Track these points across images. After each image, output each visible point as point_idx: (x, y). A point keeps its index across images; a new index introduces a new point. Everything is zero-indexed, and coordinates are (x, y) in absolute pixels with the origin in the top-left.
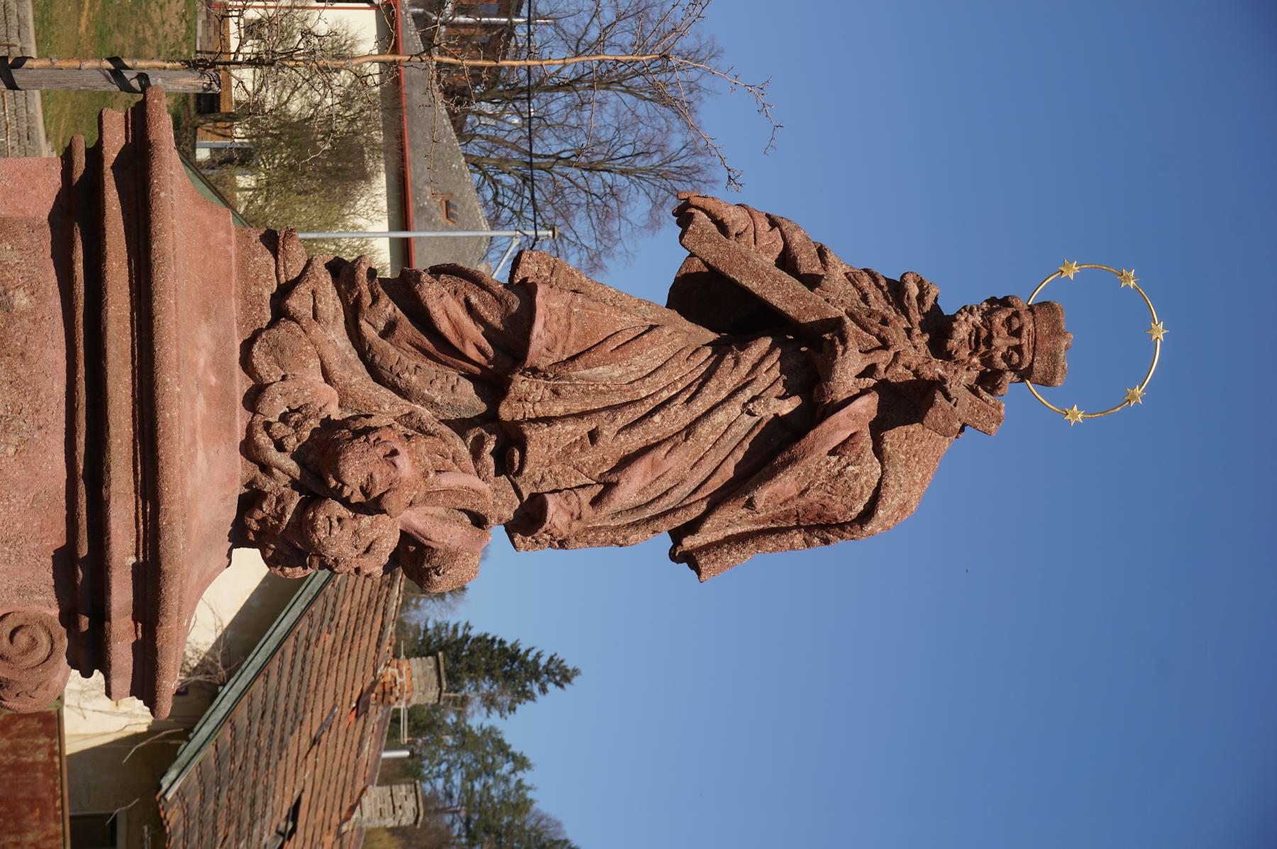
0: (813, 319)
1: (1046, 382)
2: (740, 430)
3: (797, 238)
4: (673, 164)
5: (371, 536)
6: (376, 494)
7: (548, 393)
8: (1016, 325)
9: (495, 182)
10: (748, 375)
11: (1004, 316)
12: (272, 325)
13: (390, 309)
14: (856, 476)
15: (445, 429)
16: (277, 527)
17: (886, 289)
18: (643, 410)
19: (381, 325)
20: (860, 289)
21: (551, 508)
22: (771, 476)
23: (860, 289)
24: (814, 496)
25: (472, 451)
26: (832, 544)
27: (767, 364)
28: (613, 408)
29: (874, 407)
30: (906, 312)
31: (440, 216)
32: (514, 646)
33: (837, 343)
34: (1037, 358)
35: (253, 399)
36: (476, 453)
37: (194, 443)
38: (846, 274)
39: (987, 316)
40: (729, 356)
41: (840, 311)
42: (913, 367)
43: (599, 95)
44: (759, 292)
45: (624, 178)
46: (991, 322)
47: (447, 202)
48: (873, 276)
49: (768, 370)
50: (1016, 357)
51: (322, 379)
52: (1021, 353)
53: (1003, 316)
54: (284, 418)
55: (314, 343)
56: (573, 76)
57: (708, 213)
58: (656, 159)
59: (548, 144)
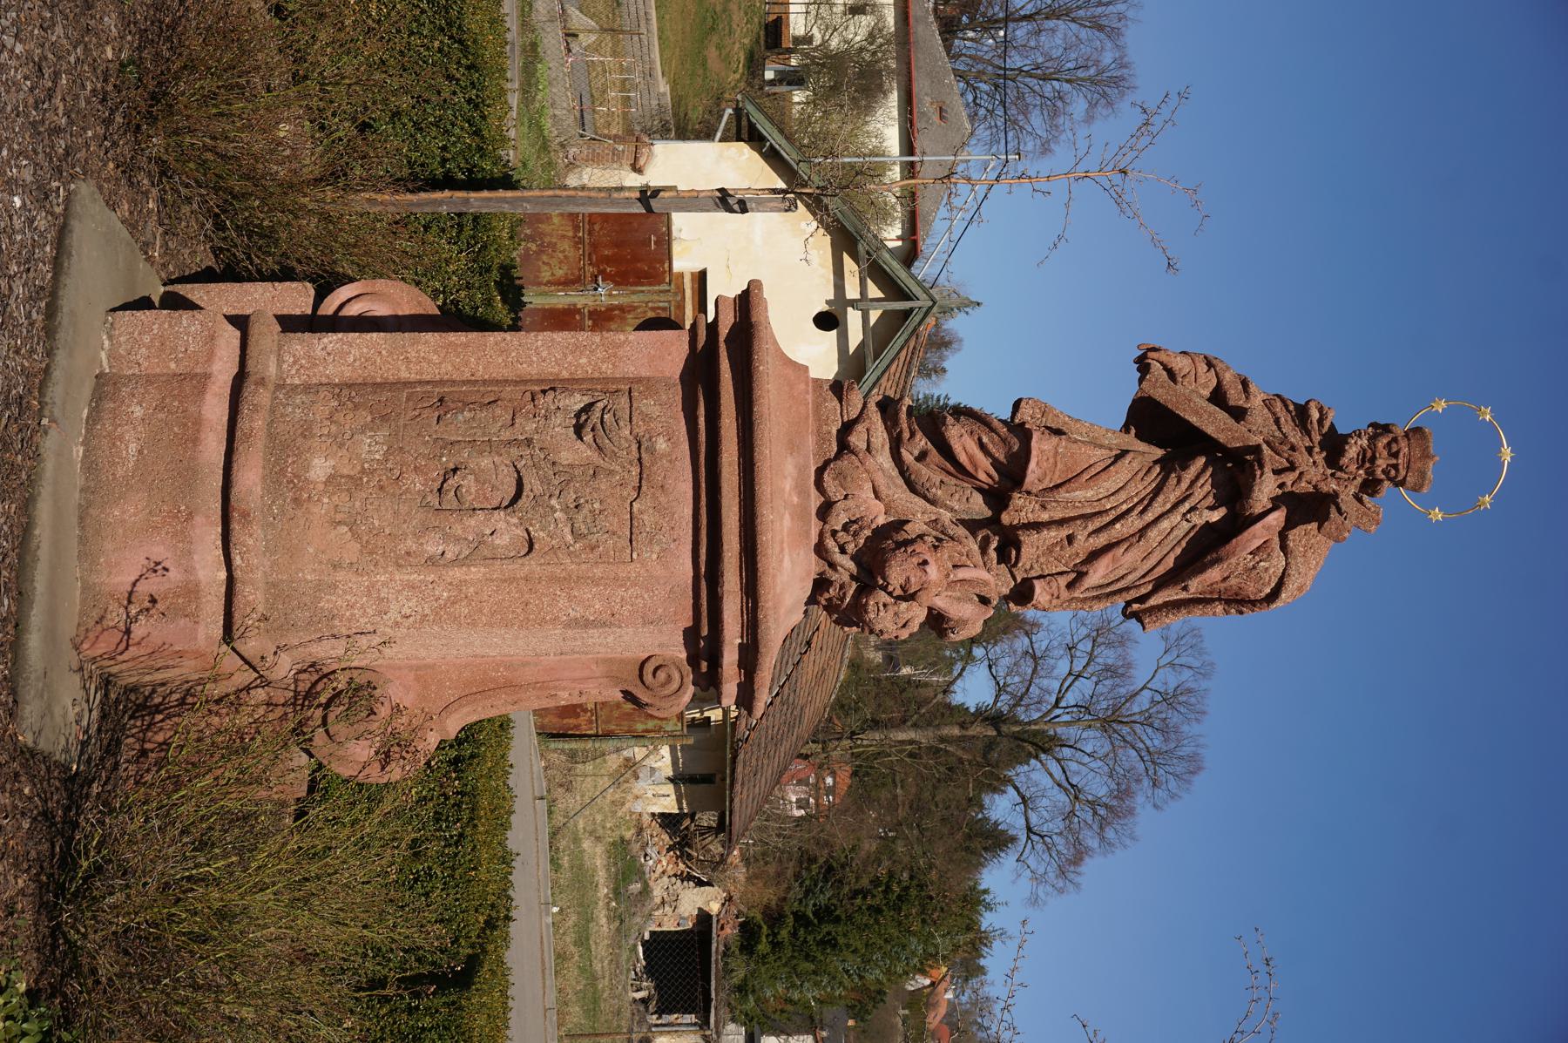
0: (1238, 445)
1: (1416, 489)
2: (1179, 533)
3: (1228, 377)
4: (1105, 75)
5: (907, 616)
6: (912, 591)
7: (1037, 506)
9: (975, 89)
10: (1187, 490)
11: (1385, 441)
12: (838, 456)
13: (923, 443)
14: (1267, 570)
15: (961, 531)
16: (840, 606)
17: (1293, 414)
18: (1107, 519)
19: (916, 453)
20: (1274, 414)
21: (1038, 590)
22: (1202, 570)
23: (1274, 414)
24: (1233, 581)
25: (980, 547)
26: (1245, 615)
28: (1086, 517)
31: (935, 118)
33: (1256, 467)
34: (1410, 474)
35: (825, 511)
36: (984, 549)
37: (782, 550)
38: (1264, 401)
39: (1373, 439)
40: (1173, 475)
41: (1258, 439)
42: (1314, 483)
43: (1051, 24)
44: (1197, 424)
45: (1068, 85)
46: (1375, 445)
47: (941, 108)
48: (1283, 401)
49: (1203, 485)
50: (1393, 472)
51: (873, 496)
52: (1397, 470)
54: (845, 528)
55: (867, 471)
56: (1034, 10)
57: (1161, 363)
58: (1092, 71)
59: (1015, 61)
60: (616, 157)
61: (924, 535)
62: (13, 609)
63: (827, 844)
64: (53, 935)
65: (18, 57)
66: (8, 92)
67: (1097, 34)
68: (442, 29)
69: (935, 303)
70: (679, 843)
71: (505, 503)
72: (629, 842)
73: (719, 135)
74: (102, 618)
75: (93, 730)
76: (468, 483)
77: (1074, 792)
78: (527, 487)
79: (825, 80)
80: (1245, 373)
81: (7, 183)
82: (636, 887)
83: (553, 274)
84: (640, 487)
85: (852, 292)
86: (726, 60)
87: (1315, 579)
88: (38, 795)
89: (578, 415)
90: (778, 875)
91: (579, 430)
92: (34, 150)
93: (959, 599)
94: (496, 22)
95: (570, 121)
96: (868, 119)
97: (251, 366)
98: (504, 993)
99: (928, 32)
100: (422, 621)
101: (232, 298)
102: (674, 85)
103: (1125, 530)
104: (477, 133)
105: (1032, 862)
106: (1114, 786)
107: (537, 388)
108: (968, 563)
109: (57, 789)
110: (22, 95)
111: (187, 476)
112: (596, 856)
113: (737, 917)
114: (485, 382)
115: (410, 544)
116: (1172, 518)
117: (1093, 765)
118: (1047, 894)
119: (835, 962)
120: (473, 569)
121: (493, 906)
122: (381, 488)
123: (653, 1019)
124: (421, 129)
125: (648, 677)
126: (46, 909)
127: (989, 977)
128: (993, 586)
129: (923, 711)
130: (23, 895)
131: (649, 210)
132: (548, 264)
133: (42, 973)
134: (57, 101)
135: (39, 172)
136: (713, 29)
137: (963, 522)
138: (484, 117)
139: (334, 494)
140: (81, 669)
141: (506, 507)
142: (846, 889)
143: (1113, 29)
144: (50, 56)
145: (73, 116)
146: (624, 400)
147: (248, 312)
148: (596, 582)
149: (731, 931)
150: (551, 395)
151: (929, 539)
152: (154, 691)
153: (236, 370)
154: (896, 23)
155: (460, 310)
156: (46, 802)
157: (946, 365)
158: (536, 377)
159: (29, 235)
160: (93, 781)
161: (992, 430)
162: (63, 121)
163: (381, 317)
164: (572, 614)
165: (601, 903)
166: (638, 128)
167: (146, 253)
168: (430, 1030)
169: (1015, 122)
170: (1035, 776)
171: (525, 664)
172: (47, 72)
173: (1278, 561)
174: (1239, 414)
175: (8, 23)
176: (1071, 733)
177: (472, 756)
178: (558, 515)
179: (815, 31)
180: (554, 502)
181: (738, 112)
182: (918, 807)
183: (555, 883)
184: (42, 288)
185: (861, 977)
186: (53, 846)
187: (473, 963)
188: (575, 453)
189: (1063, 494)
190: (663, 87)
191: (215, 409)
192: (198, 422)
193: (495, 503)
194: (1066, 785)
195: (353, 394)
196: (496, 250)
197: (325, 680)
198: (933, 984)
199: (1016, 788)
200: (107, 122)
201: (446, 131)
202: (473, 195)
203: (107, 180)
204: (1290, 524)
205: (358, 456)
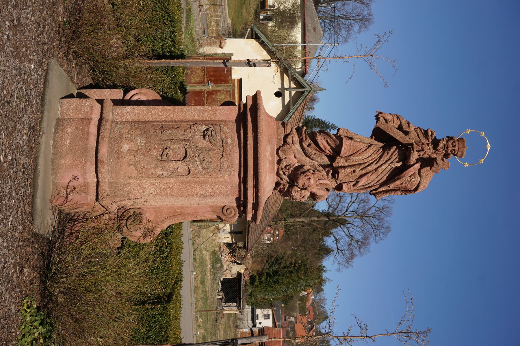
1: (460, 157)
2: (387, 170)
3: (403, 122)
5: (304, 195)
6: (305, 187)
7: (344, 161)
8: (454, 144)
9: (324, 22)
12: (284, 145)
14: (414, 181)
15: (321, 168)
18: (365, 165)
19: (307, 144)
20: (417, 133)
21: (344, 187)
22: (394, 181)
23: (417, 133)
24: (404, 185)
25: (327, 173)
27: (395, 154)
29: (419, 166)
30: (428, 139)
31: (312, 31)
32: (324, 121)
35: (279, 162)
36: (328, 174)
37: (266, 174)
39: (448, 141)
44: (394, 136)
50: (453, 152)
53: (451, 142)
54: (285, 167)
55: (292, 150)
57: (383, 117)
58: (361, 17)
59: (337, 13)
60: (215, 43)
61: (310, 170)
62: (32, 191)
63: (276, 252)
64: (44, 290)
65: (32, 22)
66: (29, 32)
67: (363, 5)
68: (162, 9)
69: (312, 89)
70: (232, 252)
71: (182, 159)
72: (217, 251)
73: (246, 37)
74: (59, 193)
75: (56, 227)
76: (170, 153)
77: (352, 237)
78: (188, 154)
79: (279, 19)
80: (409, 120)
81: (29, 61)
82: (219, 265)
83: (195, 80)
84: (223, 154)
85: (286, 86)
86: (248, 13)
87: (429, 184)
88: (40, 248)
89: (204, 132)
90: (262, 261)
91: (204, 136)
92: (38, 50)
93: (320, 189)
94: (179, 6)
95: (201, 32)
96: (292, 31)
97: (104, 116)
98: (180, 303)
99: (310, 4)
100: (156, 195)
101: (98, 94)
102: (232, 20)
103: (371, 169)
104: (173, 41)
105: (338, 258)
106: (363, 236)
107: (191, 123)
108: (323, 178)
109: (46, 245)
110: (34, 33)
111: (85, 149)
112: (207, 256)
113: (249, 274)
114: (175, 121)
115: (153, 171)
116: (386, 165)
117: (357, 229)
118: (343, 268)
119: (278, 287)
120: (172, 179)
121: (177, 277)
122: (144, 154)
123: (224, 304)
124: (156, 40)
125: (225, 212)
126: (43, 282)
127: (325, 292)
128: (330, 185)
129: (306, 212)
130: (36, 278)
131: (226, 66)
132: (194, 77)
133: (41, 301)
134: (45, 35)
135: (39, 57)
136: (244, 3)
137: (321, 165)
138: (175, 36)
139: (129, 156)
140: (53, 209)
141: (182, 160)
142: (282, 266)
143: (367, 4)
144: (42, 20)
145: (49, 39)
146: (218, 127)
147: (103, 98)
148: (209, 183)
149: (247, 278)
150: (196, 126)
151: (311, 171)
152: (75, 215)
153: (99, 117)
154: (301, 2)
155: (167, 95)
156: (42, 249)
157: (314, 106)
158: (191, 120)
159: (36, 76)
160: (56, 242)
161: (331, 137)
162: (46, 40)
163: (144, 100)
164: (202, 193)
165: (208, 270)
166: (221, 34)
167: (72, 80)
168: (158, 315)
169: (337, 32)
170: (339, 232)
171: (187, 207)
172: (41, 25)
173: (418, 179)
174: (406, 133)
175: (29, 11)
176: (351, 219)
177: (171, 232)
178: (198, 163)
179: (276, 4)
180: (196, 159)
181: (252, 29)
182: (304, 241)
183: (195, 265)
184: (40, 92)
185: (286, 292)
186: (44, 263)
187: (170, 295)
188: (203, 143)
189: (352, 158)
190: (229, 21)
191: (93, 129)
192: (88, 133)
193: (179, 159)
194: (349, 235)
195: (135, 125)
196: (179, 77)
197: (127, 212)
198: (308, 294)
199: (334, 236)
200: (60, 40)
201: (163, 40)
202: (172, 61)
203: (60, 58)
204: (422, 167)
205: (137, 144)
